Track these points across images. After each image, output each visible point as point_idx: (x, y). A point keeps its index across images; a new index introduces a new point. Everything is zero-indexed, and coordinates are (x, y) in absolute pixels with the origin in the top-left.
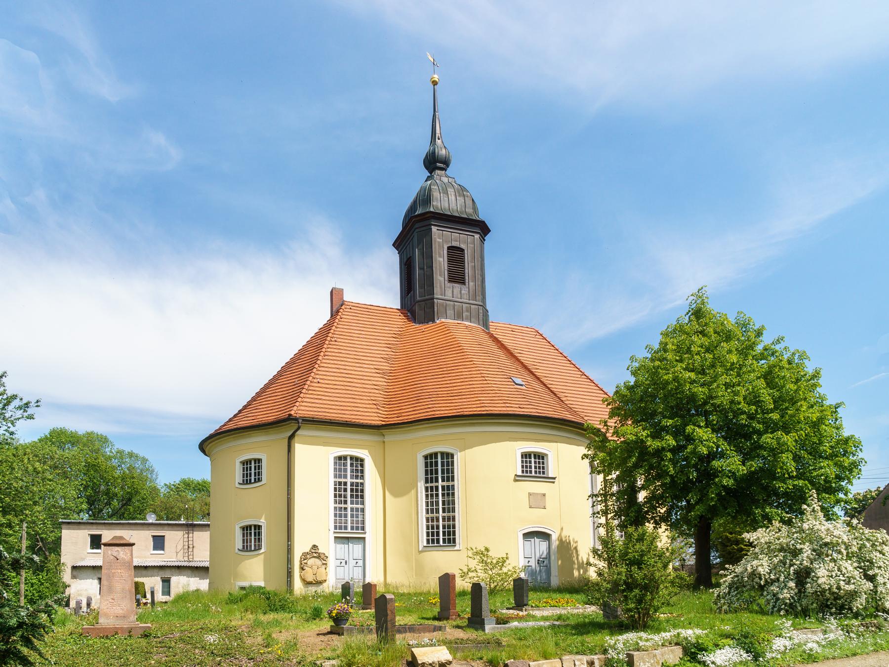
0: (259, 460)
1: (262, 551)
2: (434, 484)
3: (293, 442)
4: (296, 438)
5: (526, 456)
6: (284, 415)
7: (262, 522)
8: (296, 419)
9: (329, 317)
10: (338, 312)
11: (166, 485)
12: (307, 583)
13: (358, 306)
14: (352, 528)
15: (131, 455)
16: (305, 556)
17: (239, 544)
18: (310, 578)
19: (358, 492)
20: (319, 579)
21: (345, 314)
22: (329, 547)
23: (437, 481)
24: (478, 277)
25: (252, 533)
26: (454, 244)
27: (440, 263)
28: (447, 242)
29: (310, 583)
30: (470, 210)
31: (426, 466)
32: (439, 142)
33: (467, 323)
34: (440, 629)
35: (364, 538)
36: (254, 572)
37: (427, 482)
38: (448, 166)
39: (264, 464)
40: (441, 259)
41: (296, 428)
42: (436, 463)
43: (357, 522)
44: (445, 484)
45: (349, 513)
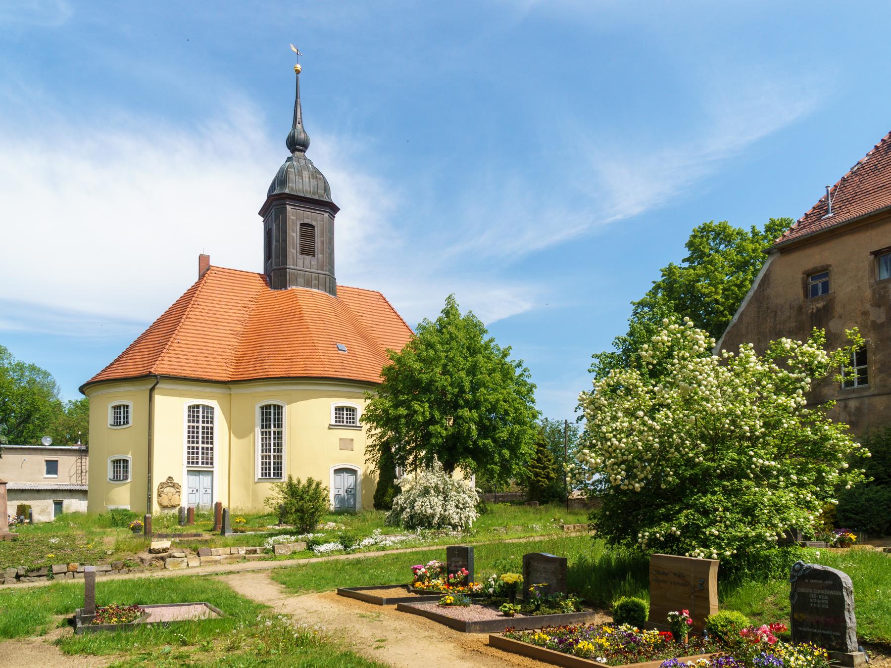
0: (127, 407)
1: (129, 480)
2: (268, 430)
4: (156, 391)
5: (339, 409)
6: (146, 372)
7: (129, 457)
8: (155, 376)
9: (197, 279)
10: (204, 276)
11: (70, 402)
12: (164, 507)
13: (223, 270)
14: (203, 463)
15: (33, 368)
16: (162, 485)
17: (110, 475)
18: (166, 503)
19: (209, 435)
21: (210, 279)
23: (270, 427)
24: (327, 250)
25: (120, 464)
27: (293, 237)
28: (300, 219)
30: (321, 191)
31: (263, 415)
32: (299, 126)
33: (316, 290)
36: (122, 498)
37: (262, 428)
38: (307, 148)
40: (294, 234)
41: (155, 382)
42: (270, 412)
43: (207, 459)
44: (276, 429)
45: (200, 451)
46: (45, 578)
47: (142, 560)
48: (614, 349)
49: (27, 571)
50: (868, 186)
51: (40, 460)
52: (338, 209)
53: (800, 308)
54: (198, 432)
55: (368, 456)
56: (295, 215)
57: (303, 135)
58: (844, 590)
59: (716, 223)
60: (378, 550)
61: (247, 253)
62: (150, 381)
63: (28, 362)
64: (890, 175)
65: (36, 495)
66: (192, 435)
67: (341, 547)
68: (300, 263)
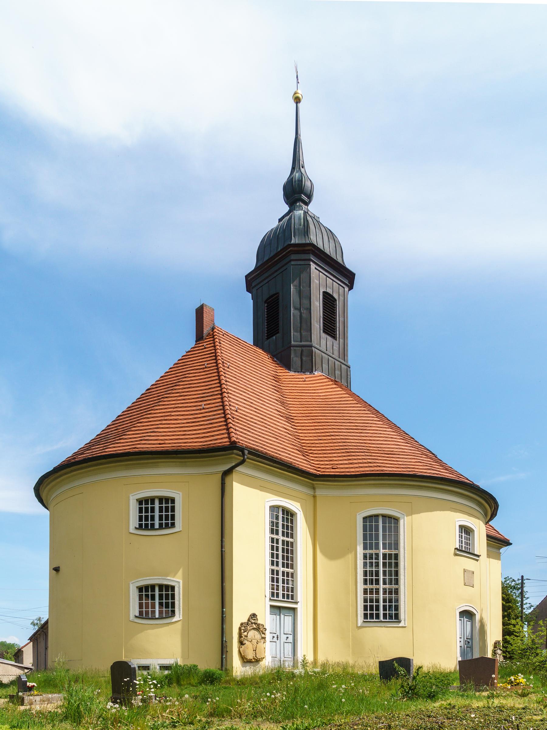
3: (227, 480)
7: (177, 580)
8: (242, 450)
12: (245, 661)
16: (244, 627)
17: (134, 610)
18: (250, 656)
22: (266, 619)
23: (377, 548)
35: (294, 610)
36: (163, 646)
44: (387, 551)
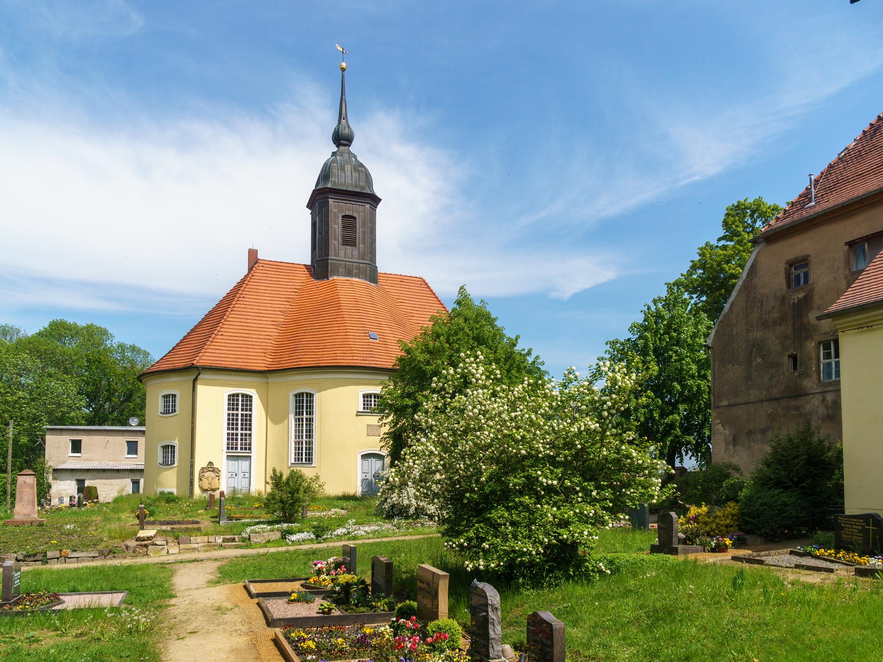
0: (174, 396)
2: (301, 417)
4: (198, 381)
5: (366, 396)
7: (176, 443)
8: (197, 368)
13: (270, 263)
14: (241, 449)
15: (133, 349)
16: (203, 470)
17: (160, 460)
18: (206, 487)
20: (213, 487)
21: (258, 273)
24: (368, 240)
25: (168, 449)
26: (348, 213)
28: (342, 212)
29: (206, 490)
30: (362, 184)
32: (343, 121)
34: (831, 571)
36: (169, 482)
39: (178, 399)
41: (197, 373)
44: (308, 416)
45: (239, 437)
46: (40, 563)
47: (127, 547)
48: (630, 336)
49: (25, 556)
50: (849, 174)
51: (121, 442)
52: (380, 200)
53: (783, 299)
54: (237, 420)
55: (382, 444)
56: (337, 208)
57: (347, 129)
58: (489, 607)
59: (751, 200)
60: (349, 539)
61: (293, 242)
62: (193, 372)
63: (128, 342)
64: (872, 160)
65: (116, 475)
66: (232, 422)
67: (313, 536)
68: (342, 253)
